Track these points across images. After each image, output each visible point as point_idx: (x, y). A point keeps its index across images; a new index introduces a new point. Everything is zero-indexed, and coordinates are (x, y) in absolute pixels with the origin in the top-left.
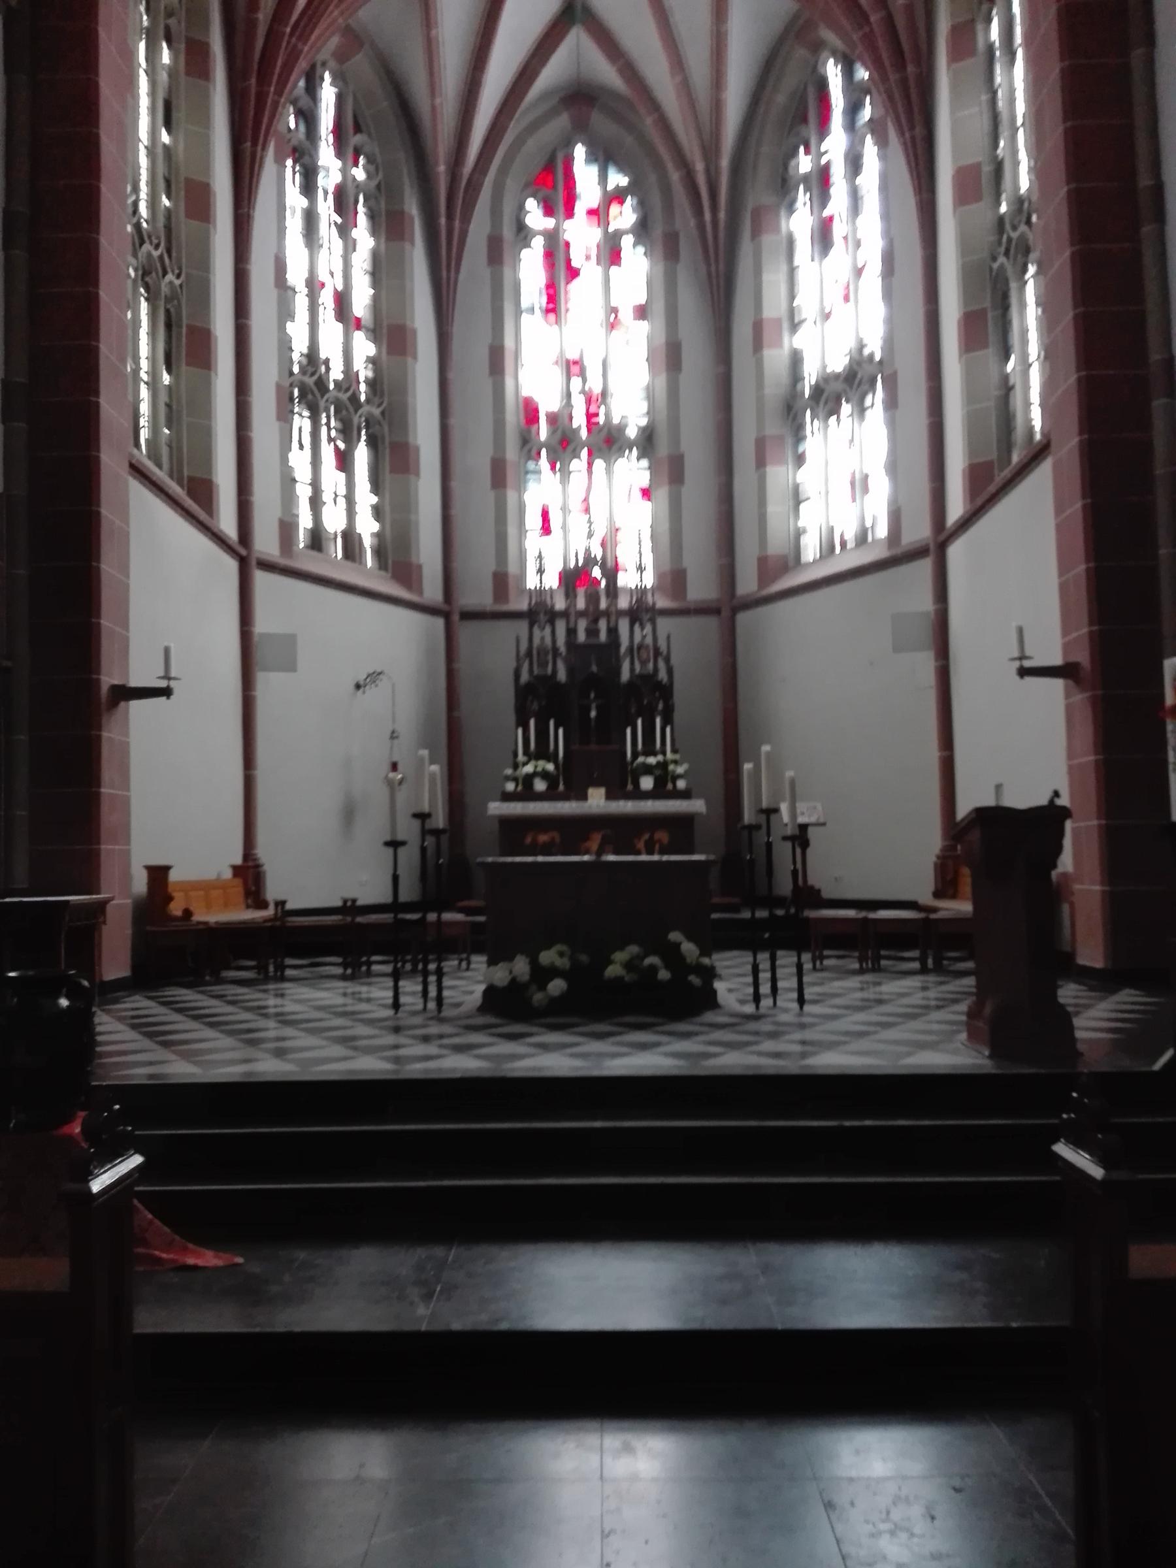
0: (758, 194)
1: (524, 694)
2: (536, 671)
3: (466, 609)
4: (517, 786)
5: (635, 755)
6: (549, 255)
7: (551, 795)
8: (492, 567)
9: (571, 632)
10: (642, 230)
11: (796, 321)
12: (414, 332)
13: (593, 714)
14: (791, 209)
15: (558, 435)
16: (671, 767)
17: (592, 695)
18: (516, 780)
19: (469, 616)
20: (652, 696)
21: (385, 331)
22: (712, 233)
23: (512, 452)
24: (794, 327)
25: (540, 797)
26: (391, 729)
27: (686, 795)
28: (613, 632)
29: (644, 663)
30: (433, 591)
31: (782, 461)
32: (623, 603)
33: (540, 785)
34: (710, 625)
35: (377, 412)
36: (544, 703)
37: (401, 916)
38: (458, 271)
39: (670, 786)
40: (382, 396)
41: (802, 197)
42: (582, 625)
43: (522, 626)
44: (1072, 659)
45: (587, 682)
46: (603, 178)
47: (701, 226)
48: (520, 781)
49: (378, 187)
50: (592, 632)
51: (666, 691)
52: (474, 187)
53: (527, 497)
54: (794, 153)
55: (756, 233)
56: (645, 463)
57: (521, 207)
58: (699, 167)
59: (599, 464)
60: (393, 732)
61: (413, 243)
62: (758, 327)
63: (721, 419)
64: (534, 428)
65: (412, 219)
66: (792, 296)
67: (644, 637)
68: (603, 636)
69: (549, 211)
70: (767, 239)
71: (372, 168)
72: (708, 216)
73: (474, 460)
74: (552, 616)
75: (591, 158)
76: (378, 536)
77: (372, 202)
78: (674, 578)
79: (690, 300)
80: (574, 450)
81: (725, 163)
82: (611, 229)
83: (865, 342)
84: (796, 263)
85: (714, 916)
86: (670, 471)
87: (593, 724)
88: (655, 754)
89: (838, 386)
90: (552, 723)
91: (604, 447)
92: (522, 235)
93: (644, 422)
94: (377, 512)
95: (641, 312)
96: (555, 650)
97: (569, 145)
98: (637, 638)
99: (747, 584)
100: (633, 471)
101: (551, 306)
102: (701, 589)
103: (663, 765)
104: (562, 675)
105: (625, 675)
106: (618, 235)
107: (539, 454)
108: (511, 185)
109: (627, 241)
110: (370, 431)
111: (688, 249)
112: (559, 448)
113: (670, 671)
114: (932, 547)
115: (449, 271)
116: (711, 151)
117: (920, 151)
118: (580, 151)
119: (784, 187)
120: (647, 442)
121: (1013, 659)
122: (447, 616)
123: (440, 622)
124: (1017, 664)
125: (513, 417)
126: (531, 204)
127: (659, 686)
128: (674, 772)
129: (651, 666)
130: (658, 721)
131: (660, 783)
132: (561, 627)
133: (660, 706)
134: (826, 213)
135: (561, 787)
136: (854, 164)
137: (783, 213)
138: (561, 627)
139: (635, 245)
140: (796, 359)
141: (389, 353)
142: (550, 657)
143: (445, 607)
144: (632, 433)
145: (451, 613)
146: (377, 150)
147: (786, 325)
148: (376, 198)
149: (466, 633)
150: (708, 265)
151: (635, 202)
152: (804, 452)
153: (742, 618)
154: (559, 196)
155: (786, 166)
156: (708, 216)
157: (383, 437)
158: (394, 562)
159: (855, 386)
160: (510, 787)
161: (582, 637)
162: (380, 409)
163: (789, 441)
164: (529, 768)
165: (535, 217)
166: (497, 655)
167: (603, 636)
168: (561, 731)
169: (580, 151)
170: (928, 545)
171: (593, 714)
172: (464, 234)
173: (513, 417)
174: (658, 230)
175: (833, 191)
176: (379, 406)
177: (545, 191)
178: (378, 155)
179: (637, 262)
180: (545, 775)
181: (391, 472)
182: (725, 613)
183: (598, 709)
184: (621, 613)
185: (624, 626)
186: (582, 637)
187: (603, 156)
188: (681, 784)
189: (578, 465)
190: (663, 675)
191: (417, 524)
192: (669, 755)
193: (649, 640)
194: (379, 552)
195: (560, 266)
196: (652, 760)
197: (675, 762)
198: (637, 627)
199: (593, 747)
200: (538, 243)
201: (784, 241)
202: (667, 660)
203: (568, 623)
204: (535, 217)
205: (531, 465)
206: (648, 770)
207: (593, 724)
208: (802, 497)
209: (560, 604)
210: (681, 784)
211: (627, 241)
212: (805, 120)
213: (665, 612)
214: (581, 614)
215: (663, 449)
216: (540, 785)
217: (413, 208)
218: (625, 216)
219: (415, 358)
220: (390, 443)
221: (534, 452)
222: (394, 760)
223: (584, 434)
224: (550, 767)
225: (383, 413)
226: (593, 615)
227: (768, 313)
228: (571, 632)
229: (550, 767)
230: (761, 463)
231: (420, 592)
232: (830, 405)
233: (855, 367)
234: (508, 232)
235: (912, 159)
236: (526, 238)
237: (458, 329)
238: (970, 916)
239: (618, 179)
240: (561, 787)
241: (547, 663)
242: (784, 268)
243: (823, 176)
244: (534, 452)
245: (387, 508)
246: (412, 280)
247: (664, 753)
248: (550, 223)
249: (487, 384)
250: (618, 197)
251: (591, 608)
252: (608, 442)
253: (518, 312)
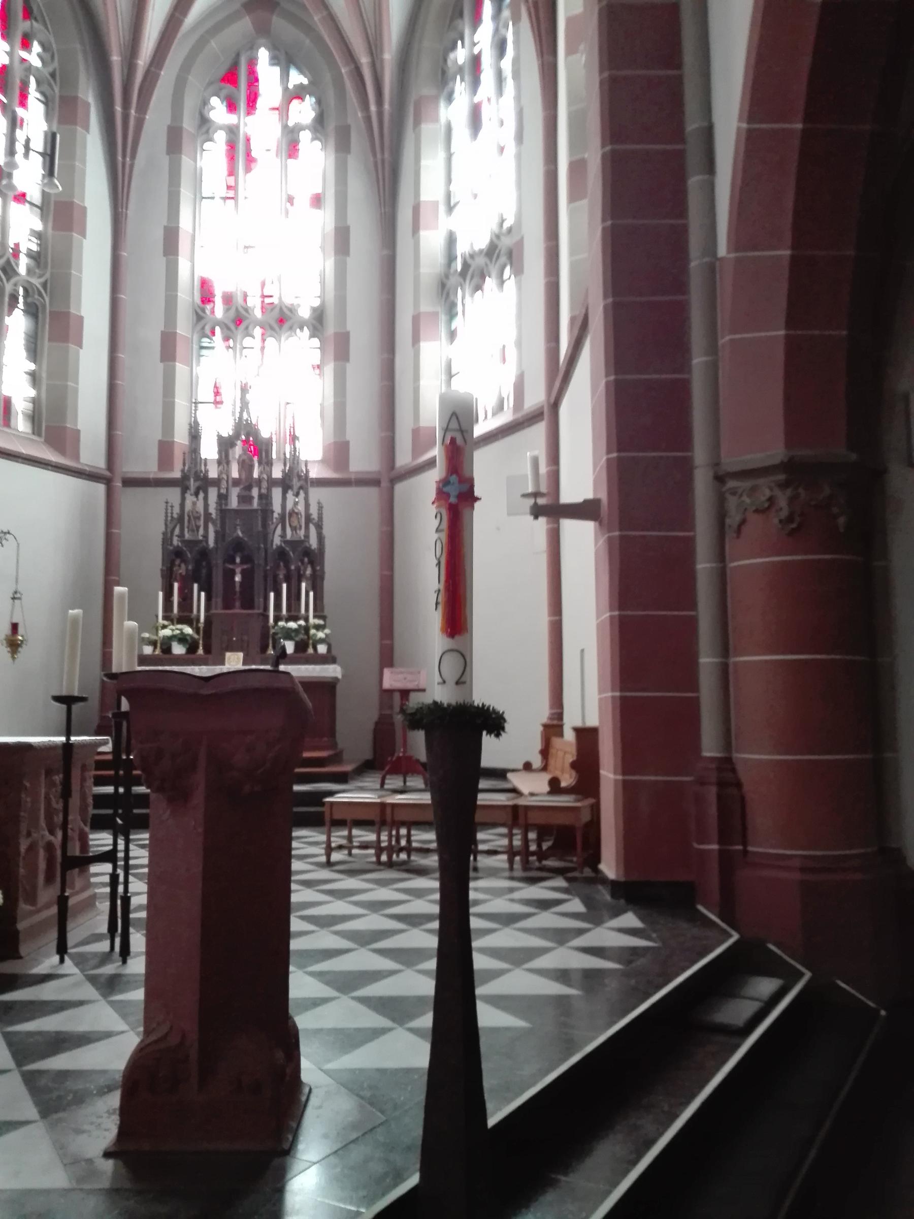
0: (421, 88)
1: (173, 557)
2: (187, 536)
3: (129, 475)
4: (154, 651)
5: (277, 619)
6: (232, 147)
7: (191, 656)
8: (159, 436)
9: (223, 498)
10: (319, 124)
11: (452, 204)
12: (84, 210)
13: (238, 578)
14: (450, 99)
15: (232, 313)
16: (313, 631)
17: (238, 560)
18: (154, 643)
19: (129, 482)
20: (301, 563)
21: (52, 208)
22: (376, 125)
23: (183, 327)
24: (450, 209)
25: (179, 660)
26: (14, 589)
27: (328, 659)
28: (265, 498)
29: (294, 529)
30: (92, 454)
31: (435, 337)
32: (277, 473)
33: (178, 649)
34: (371, 494)
35: (36, 282)
36: (190, 567)
37: (112, 772)
38: (133, 157)
39: (311, 651)
40: (46, 267)
41: (460, 88)
42: (235, 493)
43: (173, 495)
44: (598, 496)
45: (234, 549)
46: (285, 76)
47: (368, 119)
48: (159, 645)
49: (53, 75)
50: (245, 498)
51: (314, 558)
52: (151, 77)
53: (198, 370)
54: (454, 47)
55: (417, 123)
56: (316, 342)
57: (205, 102)
58: (364, 61)
59: (270, 341)
60: (16, 592)
61: (87, 128)
62: (416, 209)
63: (378, 310)
64: (208, 307)
65: (88, 105)
66: (449, 181)
67: (296, 504)
68: (255, 504)
69: (232, 107)
70: (426, 128)
71: (47, 56)
72: (373, 108)
73: (146, 333)
74: (205, 483)
75: (275, 60)
76: (35, 401)
77: (45, 88)
78: (339, 452)
79: (359, 187)
80: (247, 328)
81: (389, 56)
82: (291, 123)
83: (504, 217)
84: (452, 151)
85: (297, 788)
86: (339, 349)
87: (238, 589)
88: (295, 619)
89: (481, 261)
90: (196, 586)
91: (276, 326)
92: (204, 129)
93: (317, 303)
94: (34, 377)
95: (317, 201)
96: (207, 515)
97: (253, 47)
98: (289, 506)
99: (404, 459)
100: (303, 347)
101: (231, 194)
102: (363, 461)
103: (307, 629)
104: (211, 543)
105: (277, 541)
106: (298, 128)
107: (213, 333)
108: (194, 82)
109: (305, 137)
110: (30, 300)
111: (357, 140)
112: (232, 327)
113: (321, 538)
114: (546, 410)
115: (124, 156)
116: (374, 47)
117: (542, 15)
118: (263, 55)
119: (443, 78)
120: (317, 322)
121: (525, 496)
122: (108, 482)
123: (101, 488)
124: (531, 501)
125: (187, 294)
126: (215, 101)
127: (307, 552)
128: (315, 635)
129: (302, 533)
130: (304, 585)
131: (301, 647)
132: (213, 493)
133: (309, 571)
134: (476, 99)
135: (201, 651)
136: (500, 47)
137: (442, 104)
138: (213, 493)
139: (313, 139)
140: (451, 240)
141: (54, 228)
142: (202, 523)
143: (108, 473)
144: (305, 313)
145: (112, 479)
146: (52, 40)
147: (442, 208)
148: (50, 85)
149: (129, 499)
150: (375, 155)
151: (313, 100)
152: (456, 329)
153: (399, 488)
154: (238, 85)
155: (445, 60)
156: (373, 108)
157: (44, 306)
158: (47, 427)
159: (494, 259)
160: (148, 650)
161: (234, 503)
162: (42, 280)
163: (443, 318)
164: (167, 632)
165: (218, 112)
166: (148, 521)
167: (255, 504)
168: (203, 594)
169: (263, 55)
170: (543, 407)
171: (238, 578)
172: (140, 123)
173: (187, 294)
174: (331, 125)
175: (483, 77)
176: (40, 276)
177: (228, 88)
178: (54, 46)
179: (315, 157)
180: (182, 639)
181: (50, 340)
182: (385, 484)
183: (243, 573)
184: (273, 483)
185: (277, 493)
186: (234, 503)
187: (285, 59)
188: (322, 649)
189: (253, 341)
190: (313, 543)
191: (76, 391)
192: (312, 621)
193: (301, 508)
194: (34, 418)
195: (238, 153)
196: (292, 625)
197: (318, 627)
198: (290, 495)
199: (237, 611)
200: (221, 137)
201: (443, 130)
202: (319, 527)
203: (219, 490)
204: (218, 112)
205: (205, 342)
206: (288, 634)
207: (238, 589)
208: (453, 372)
209: (213, 474)
210: (322, 649)
211: (305, 137)
212: (461, 15)
213: (321, 483)
214: (236, 482)
215: (331, 329)
216: (178, 649)
217: (89, 95)
218: (304, 111)
219: (83, 234)
220: (50, 312)
221: (208, 330)
222: (15, 621)
223: (258, 313)
224: (188, 630)
225: (44, 285)
226: (246, 483)
227: (424, 197)
228: (223, 498)
229: (188, 630)
230: (416, 340)
231: (77, 457)
232: (476, 280)
233: (495, 239)
234: (188, 124)
235: (535, 24)
236: (207, 132)
237: (132, 210)
238: (132, 831)
239: (297, 78)
240: (201, 651)
241: (198, 528)
242: (442, 155)
243: (476, 62)
244: (208, 330)
245: (44, 375)
246: (84, 162)
247: (306, 619)
248: (232, 119)
249: (160, 262)
250: (298, 94)
251: (243, 476)
252: (281, 320)
253: (198, 197)
